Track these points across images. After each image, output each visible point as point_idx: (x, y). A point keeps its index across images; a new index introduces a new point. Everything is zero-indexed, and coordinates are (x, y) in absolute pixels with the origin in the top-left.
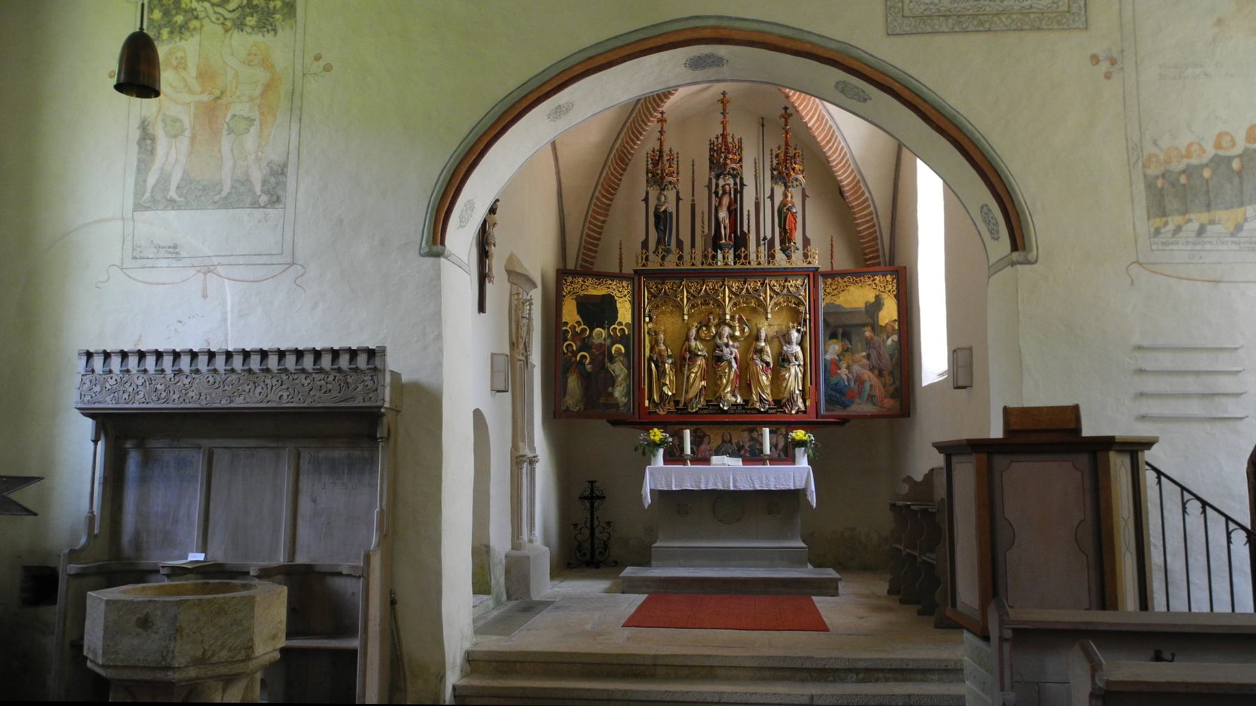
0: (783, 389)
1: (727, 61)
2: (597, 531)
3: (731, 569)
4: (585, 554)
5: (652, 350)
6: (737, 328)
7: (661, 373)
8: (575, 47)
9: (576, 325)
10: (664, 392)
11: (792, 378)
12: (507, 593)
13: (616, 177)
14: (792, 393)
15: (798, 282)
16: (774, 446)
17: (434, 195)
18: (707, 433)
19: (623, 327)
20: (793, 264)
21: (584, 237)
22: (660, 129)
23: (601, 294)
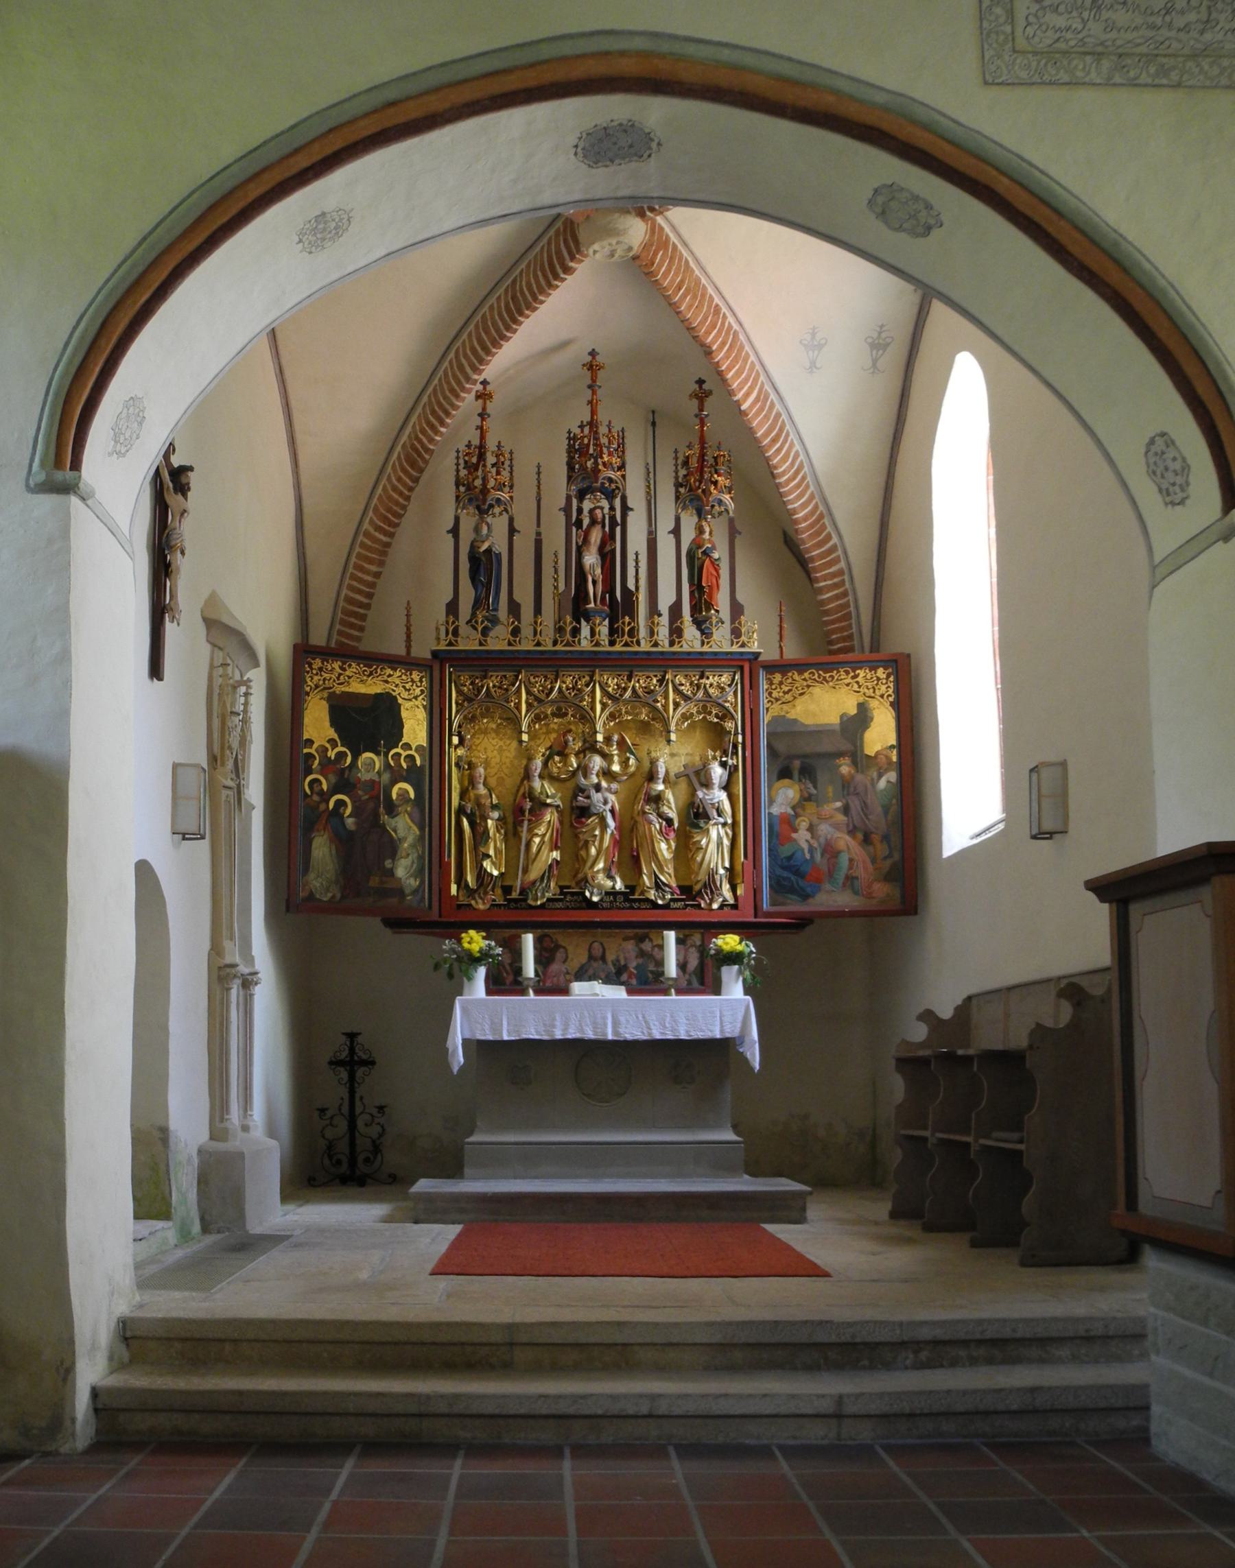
0: (695, 867)
1: (659, 144)
2: (360, 1123)
3: (607, 1180)
4: (339, 1162)
5: (463, 794)
6: (616, 758)
7: (481, 836)
8: (362, 83)
9: (328, 745)
10: (485, 870)
11: (712, 847)
12: (202, 1219)
13: (401, 494)
14: (712, 874)
15: (723, 679)
16: (682, 966)
17: (60, 368)
18: (563, 944)
20: (714, 646)
21: (342, 603)
22: (480, 411)
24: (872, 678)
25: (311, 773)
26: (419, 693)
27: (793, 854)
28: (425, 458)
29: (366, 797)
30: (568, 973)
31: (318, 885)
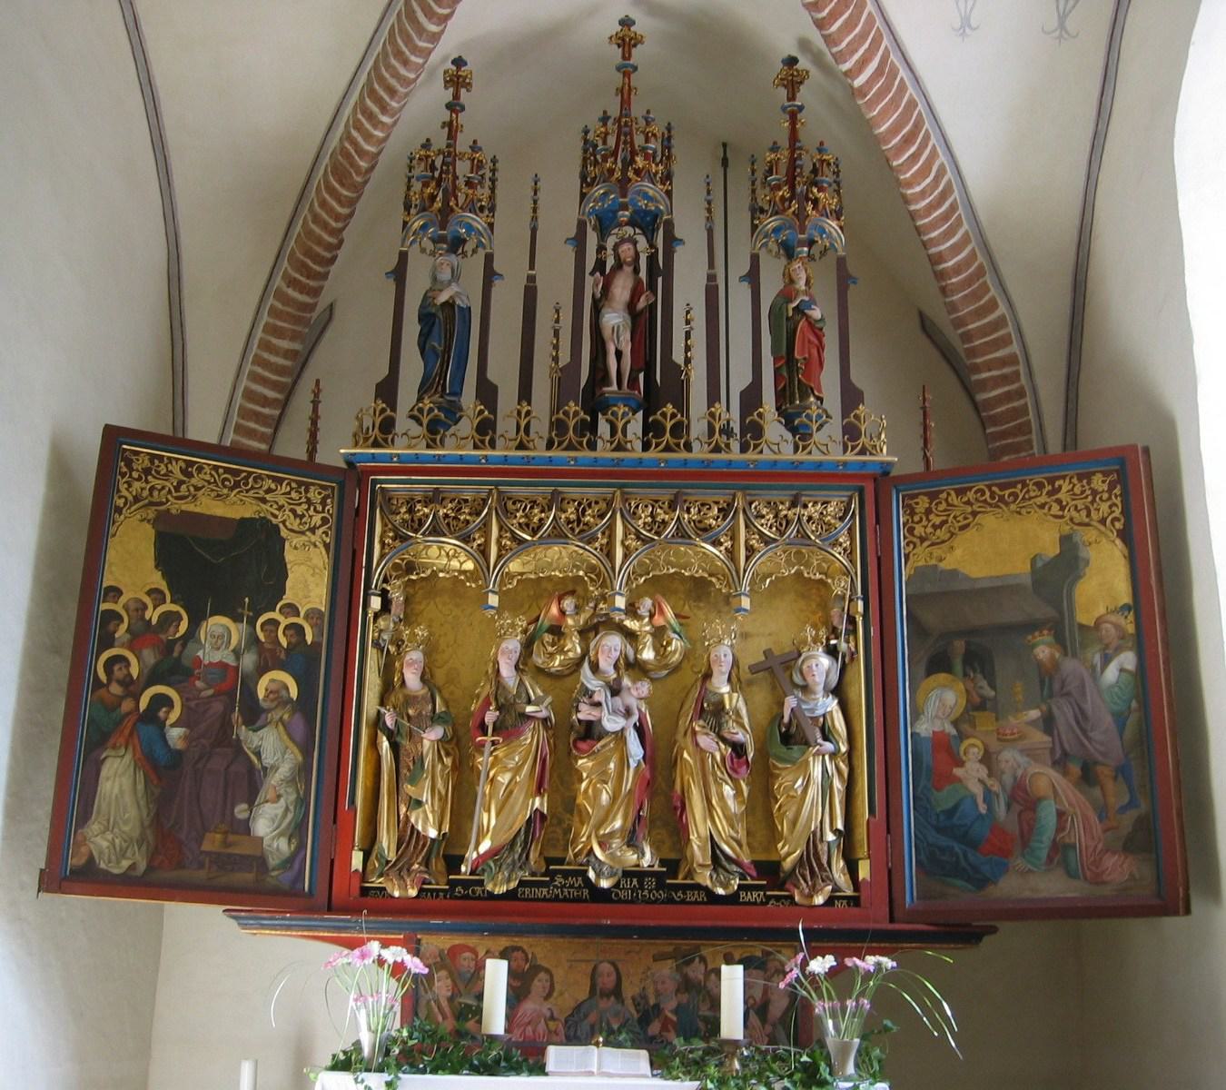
9: (147, 600)
11: (814, 791)
19: (300, 621)
23: (238, 517)
24: (1083, 492)
25: (111, 645)
26: (319, 522)
27: (956, 808)
28: (359, 167)
29: (210, 692)
30: (552, 1018)
31: (105, 844)
